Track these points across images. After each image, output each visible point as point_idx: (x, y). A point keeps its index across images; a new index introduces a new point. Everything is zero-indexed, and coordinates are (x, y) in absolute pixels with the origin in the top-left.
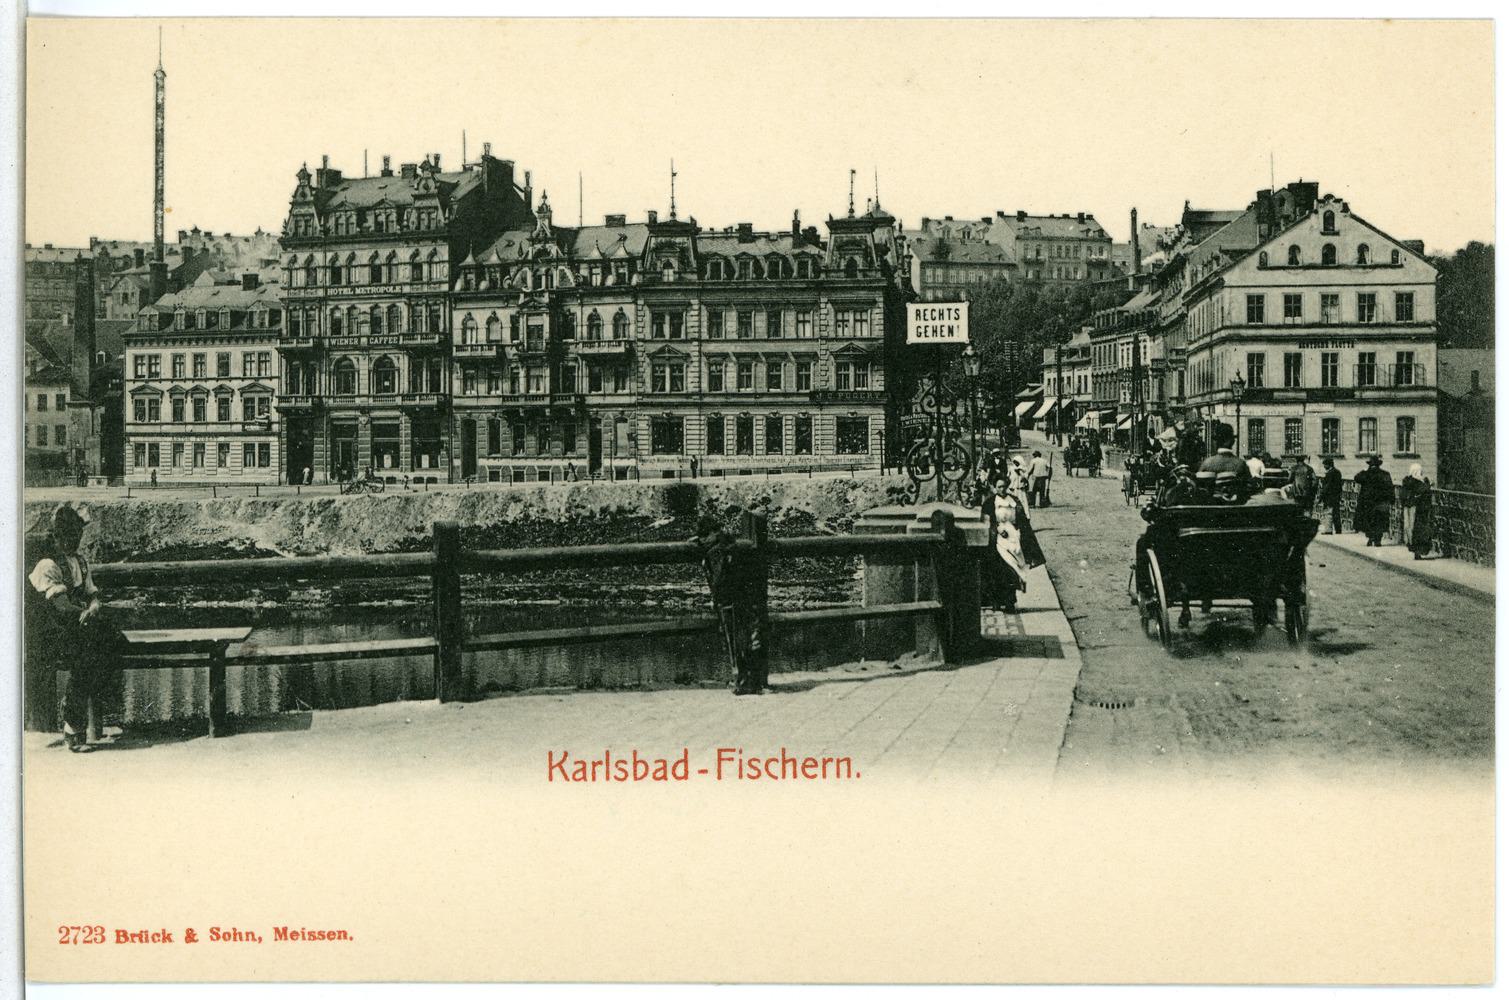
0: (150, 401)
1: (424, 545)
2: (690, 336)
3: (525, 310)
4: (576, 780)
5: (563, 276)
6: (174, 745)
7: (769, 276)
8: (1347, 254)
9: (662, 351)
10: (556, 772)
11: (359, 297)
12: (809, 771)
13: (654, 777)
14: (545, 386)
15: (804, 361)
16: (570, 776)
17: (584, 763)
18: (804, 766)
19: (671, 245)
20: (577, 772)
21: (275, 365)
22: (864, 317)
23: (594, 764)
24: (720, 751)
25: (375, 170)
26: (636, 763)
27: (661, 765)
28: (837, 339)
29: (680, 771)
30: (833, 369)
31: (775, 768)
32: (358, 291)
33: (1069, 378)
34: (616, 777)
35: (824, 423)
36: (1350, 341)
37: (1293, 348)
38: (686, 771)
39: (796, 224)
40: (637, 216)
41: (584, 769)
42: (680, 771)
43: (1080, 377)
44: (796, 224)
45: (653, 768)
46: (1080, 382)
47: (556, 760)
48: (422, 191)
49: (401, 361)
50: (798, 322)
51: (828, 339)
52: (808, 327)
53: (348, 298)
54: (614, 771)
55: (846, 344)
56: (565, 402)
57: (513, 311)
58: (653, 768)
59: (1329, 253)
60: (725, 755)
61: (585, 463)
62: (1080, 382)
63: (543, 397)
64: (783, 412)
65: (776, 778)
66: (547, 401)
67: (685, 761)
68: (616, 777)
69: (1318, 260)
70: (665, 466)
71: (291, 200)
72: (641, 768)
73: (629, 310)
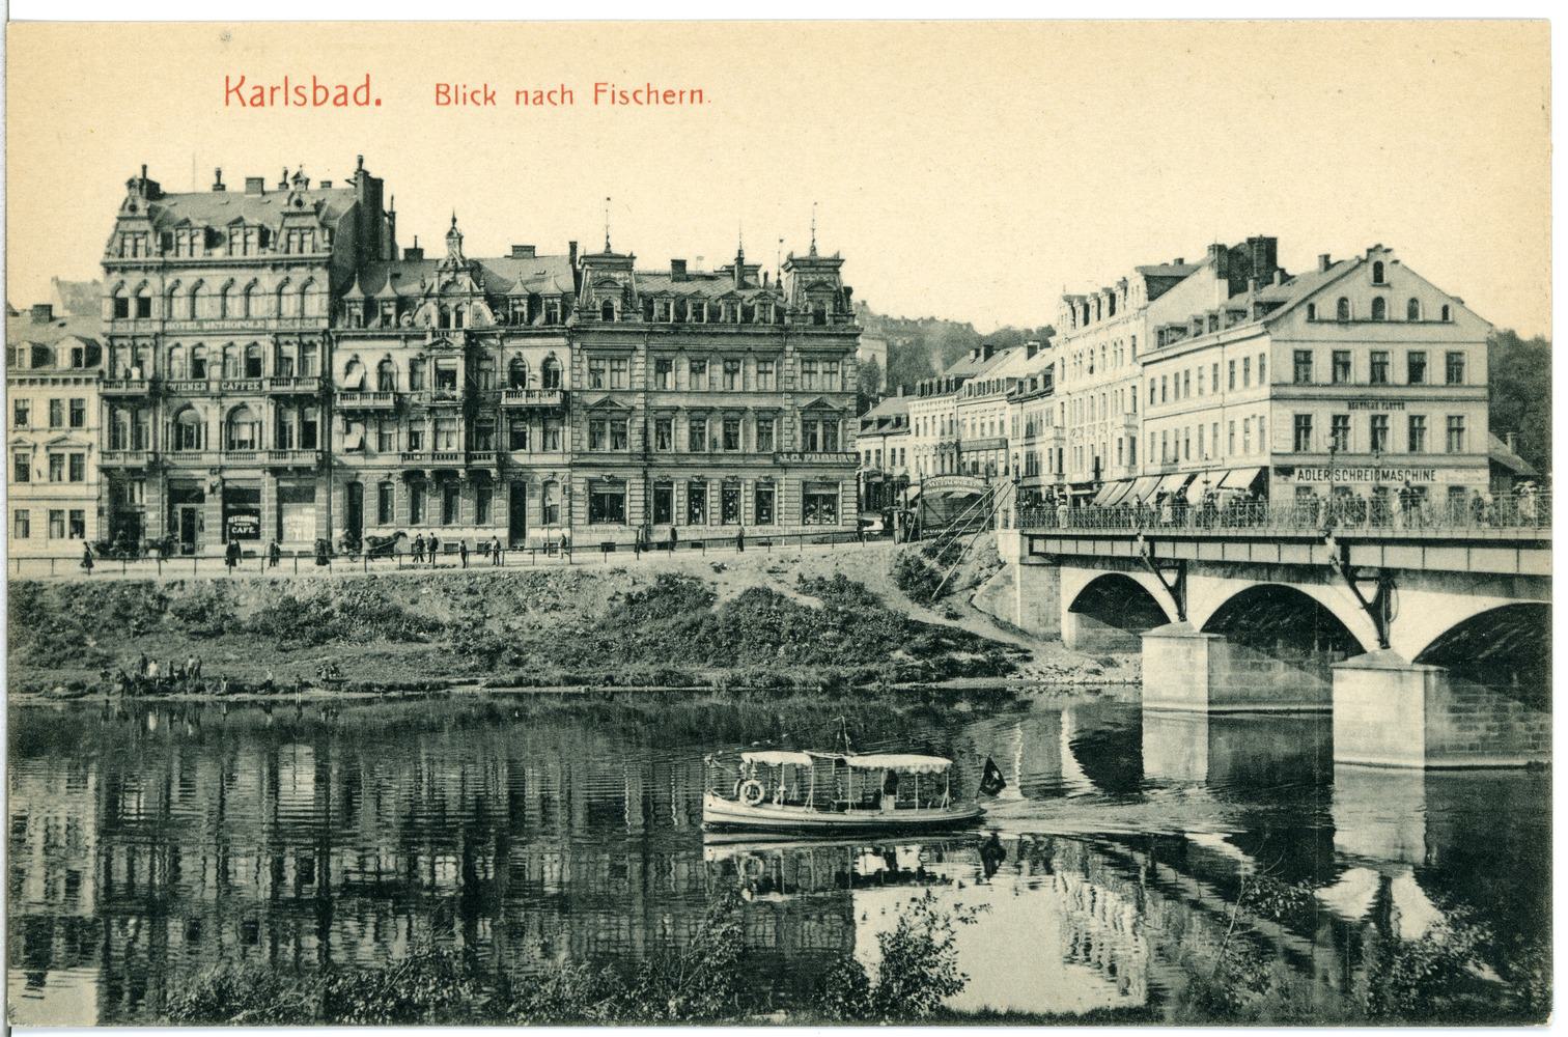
0: (72, 456)
2: (635, 387)
3: (434, 352)
5: (478, 315)
6: (1459, 592)
8: (1397, 308)
9: (602, 403)
11: (209, 334)
14: (458, 442)
15: (766, 419)
18: (665, 96)
19: (612, 281)
21: (94, 413)
22: (622, 367)
25: (205, 185)
28: (804, 393)
29: (362, 97)
30: (799, 426)
32: (206, 326)
33: (878, 451)
35: (787, 491)
36: (1400, 402)
37: (1342, 409)
39: (740, 260)
40: (552, 246)
42: (362, 97)
43: (893, 450)
44: (740, 260)
46: (893, 456)
48: (293, 209)
49: (264, 411)
50: (759, 372)
51: (793, 393)
52: (771, 378)
53: (193, 333)
55: (813, 399)
56: (451, 463)
57: (413, 354)
59: (1378, 303)
61: (503, 533)
62: (893, 456)
63: (454, 456)
64: (741, 474)
66: (461, 461)
69: (1368, 314)
70: (604, 538)
71: (117, 214)
73: (564, 357)
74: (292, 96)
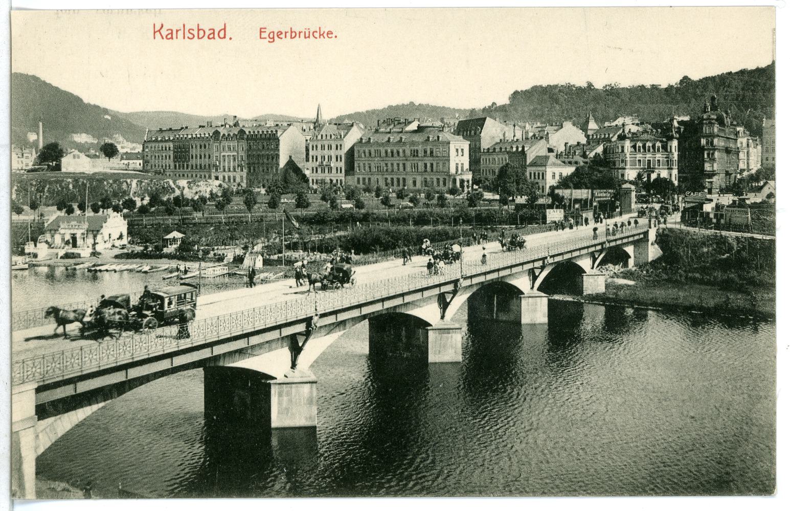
1: (204, 427)
4: (168, 39)
7: (711, 110)
10: (158, 34)
12: (330, 36)
13: (209, 38)
16: (164, 37)
17: (172, 30)
18: (328, 34)
20: (168, 34)
23: (177, 31)
24: (261, 29)
26: (199, 30)
27: (212, 31)
29: (222, 35)
31: (317, 35)
34: (188, 38)
38: (225, 34)
41: (172, 33)
42: (222, 35)
45: (208, 33)
47: (157, 28)
54: (187, 34)
58: (208, 33)
60: (262, 30)
65: (316, 38)
67: (225, 29)
68: (188, 38)
72: (201, 33)
74: (187, 34)
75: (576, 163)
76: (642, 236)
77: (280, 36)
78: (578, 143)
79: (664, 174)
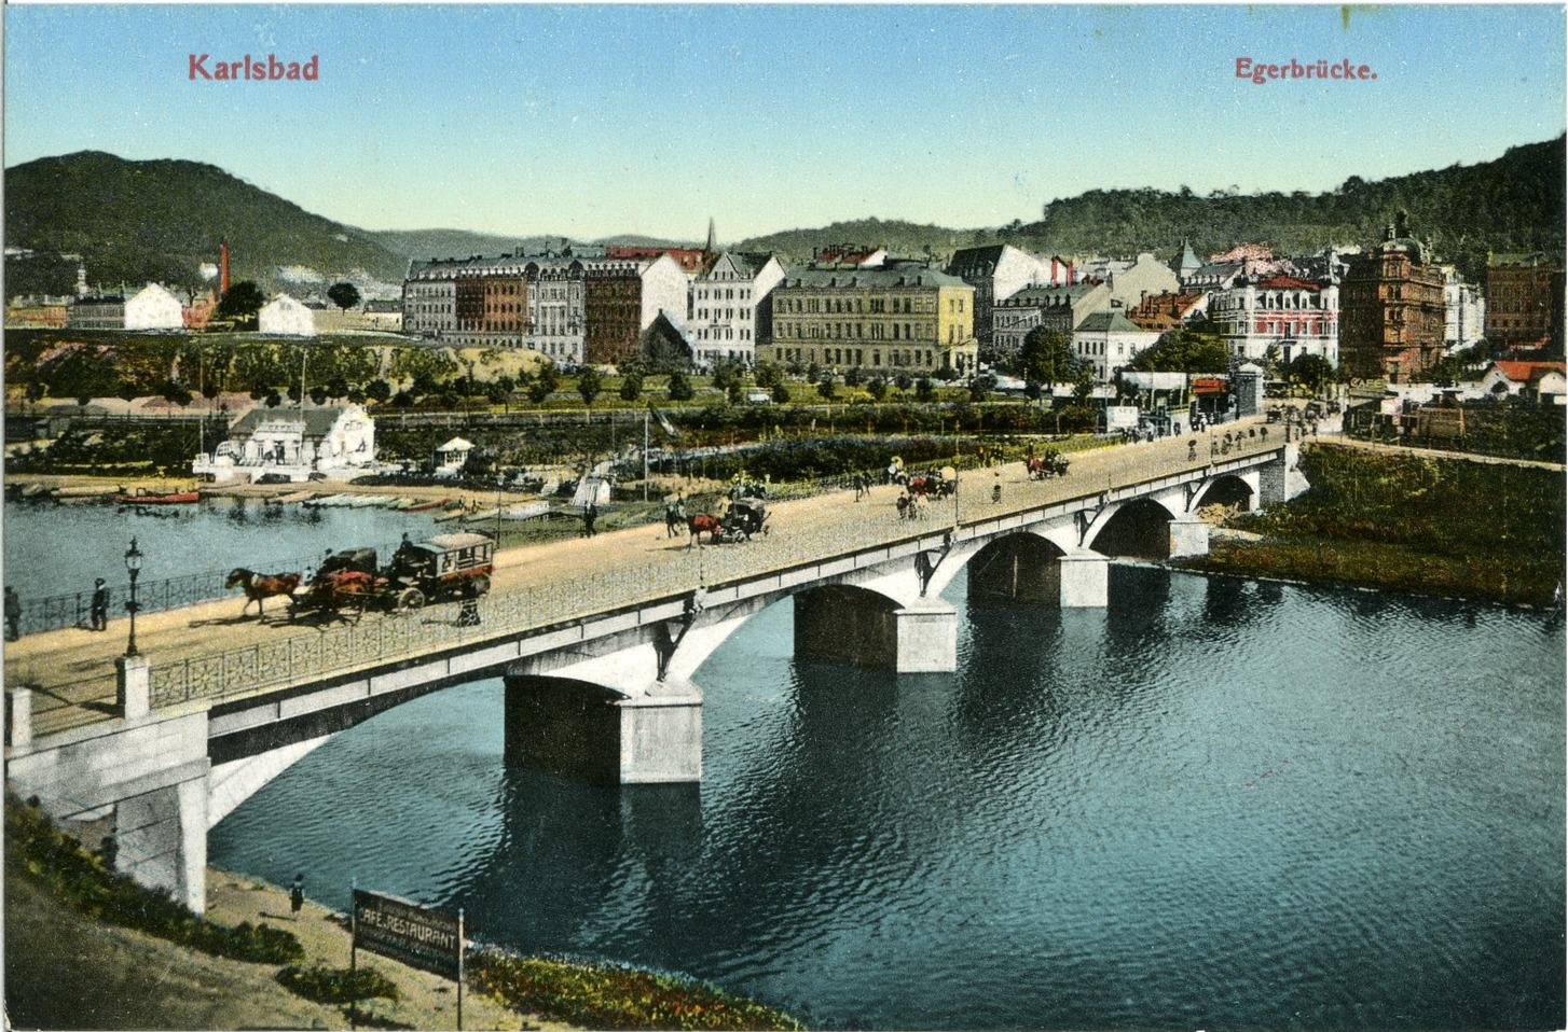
29: (310, 71)
42: (310, 71)
74: (252, 72)
75: (1160, 326)
76: (1273, 456)
77: (1274, 73)
78: (1165, 291)
79: (1314, 347)
